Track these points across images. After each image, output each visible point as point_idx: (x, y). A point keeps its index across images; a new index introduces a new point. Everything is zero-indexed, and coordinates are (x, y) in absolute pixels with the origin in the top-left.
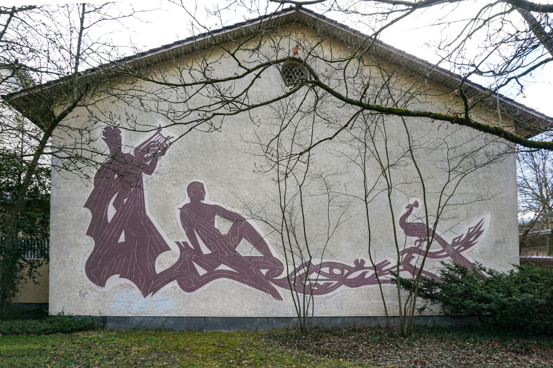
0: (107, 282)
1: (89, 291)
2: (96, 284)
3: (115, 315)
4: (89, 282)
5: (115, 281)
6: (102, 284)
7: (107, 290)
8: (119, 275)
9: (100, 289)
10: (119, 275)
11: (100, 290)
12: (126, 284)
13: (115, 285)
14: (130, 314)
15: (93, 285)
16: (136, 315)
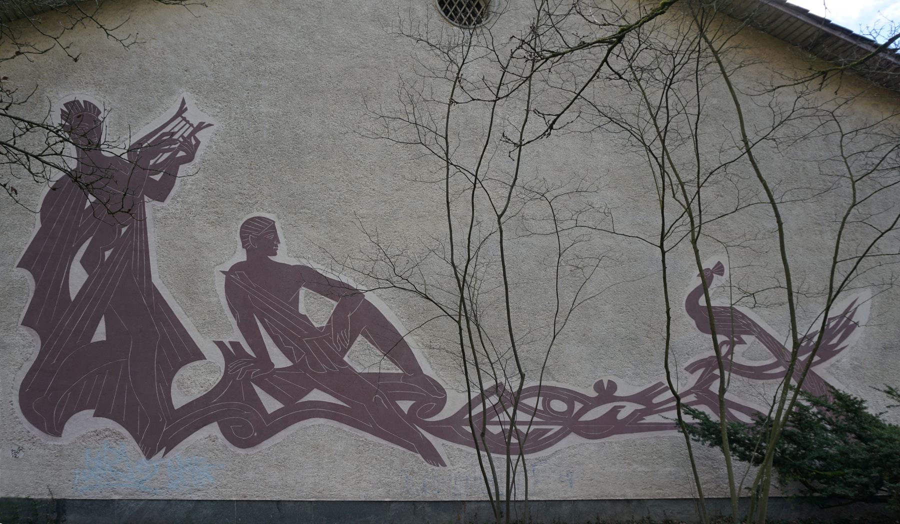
0: (68, 427)
1: (27, 446)
2: (42, 429)
3: (85, 497)
4: (27, 425)
5: (83, 423)
6: (56, 430)
7: (66, 443)
8: (92, 411)
9: (51, 441)
10: (92, 411)
11: (51, 443)
12: (107, 430)
13: (84, 432)
14: (117, 493)
15: (35, 431)
16: (130, 497)
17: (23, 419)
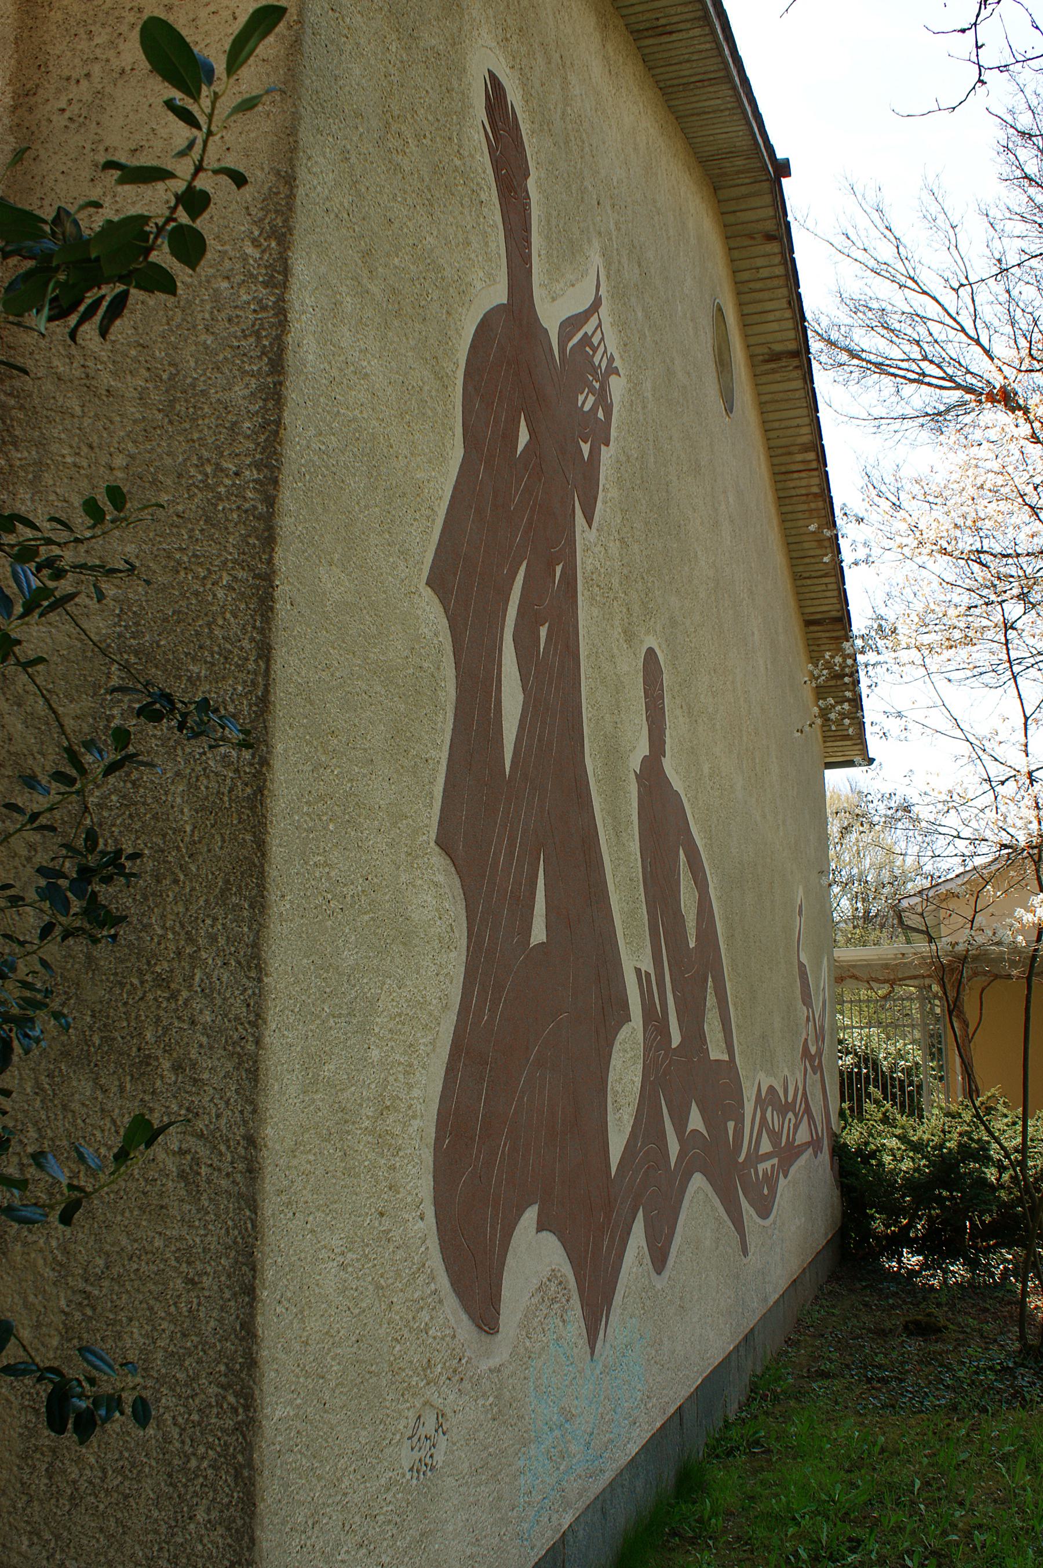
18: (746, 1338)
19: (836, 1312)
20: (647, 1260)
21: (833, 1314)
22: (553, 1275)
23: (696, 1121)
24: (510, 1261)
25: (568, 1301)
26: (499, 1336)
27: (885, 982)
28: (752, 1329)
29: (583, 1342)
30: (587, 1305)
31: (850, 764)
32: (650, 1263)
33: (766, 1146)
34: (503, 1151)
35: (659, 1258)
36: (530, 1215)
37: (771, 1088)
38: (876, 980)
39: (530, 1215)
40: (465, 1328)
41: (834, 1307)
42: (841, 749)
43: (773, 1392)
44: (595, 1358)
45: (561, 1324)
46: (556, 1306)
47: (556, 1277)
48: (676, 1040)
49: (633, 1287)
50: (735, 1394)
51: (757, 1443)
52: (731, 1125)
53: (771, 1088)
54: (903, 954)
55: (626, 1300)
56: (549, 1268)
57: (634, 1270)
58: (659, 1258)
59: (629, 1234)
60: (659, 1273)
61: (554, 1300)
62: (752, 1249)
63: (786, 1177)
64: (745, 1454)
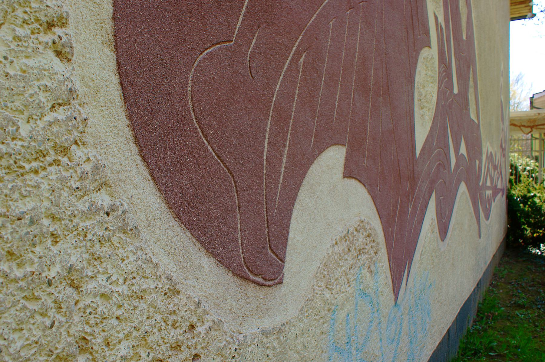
17: (139, 193)
18: (478, 284)
19: (514, 271)
20: (436, 230)
21: (512, 273)
22: (361, 227)
23: (463, 150)
24: (304, 196)
25: (376, 253)
26: (283, 289)
27: (528, 127)
28: (480, 280)
29: (388, 290)
30: (394, 258)
31: (524, 17)
32: (438, 233)
33: (489, 184)
34: (295, 60)
35: (443, 231)
36: (334, 157)
37: (491, 153)
38: (524, 126)
39: (334, 157)
40: (204, 278)
41: (511, 269)
42: (518, 10)
43: (493, 314)
44: (399, 301)
45: (368, 275)
46: (363, 257)
47: (365, 229)
48: (456, 91)
49: (428, 248)
50: (472, 316)
51: (492, 349)
52: (477, 162)
53: (491, 153)
54: (539, 114)
55: (422, 257)
56: (358, 218)
57: (429, 235)
58: (443, 231)
59: (426, 207)
60: (443, 240)
61: (361, 251)
62: (482, 235)
63: (494, 201)
64: (485, 356)
